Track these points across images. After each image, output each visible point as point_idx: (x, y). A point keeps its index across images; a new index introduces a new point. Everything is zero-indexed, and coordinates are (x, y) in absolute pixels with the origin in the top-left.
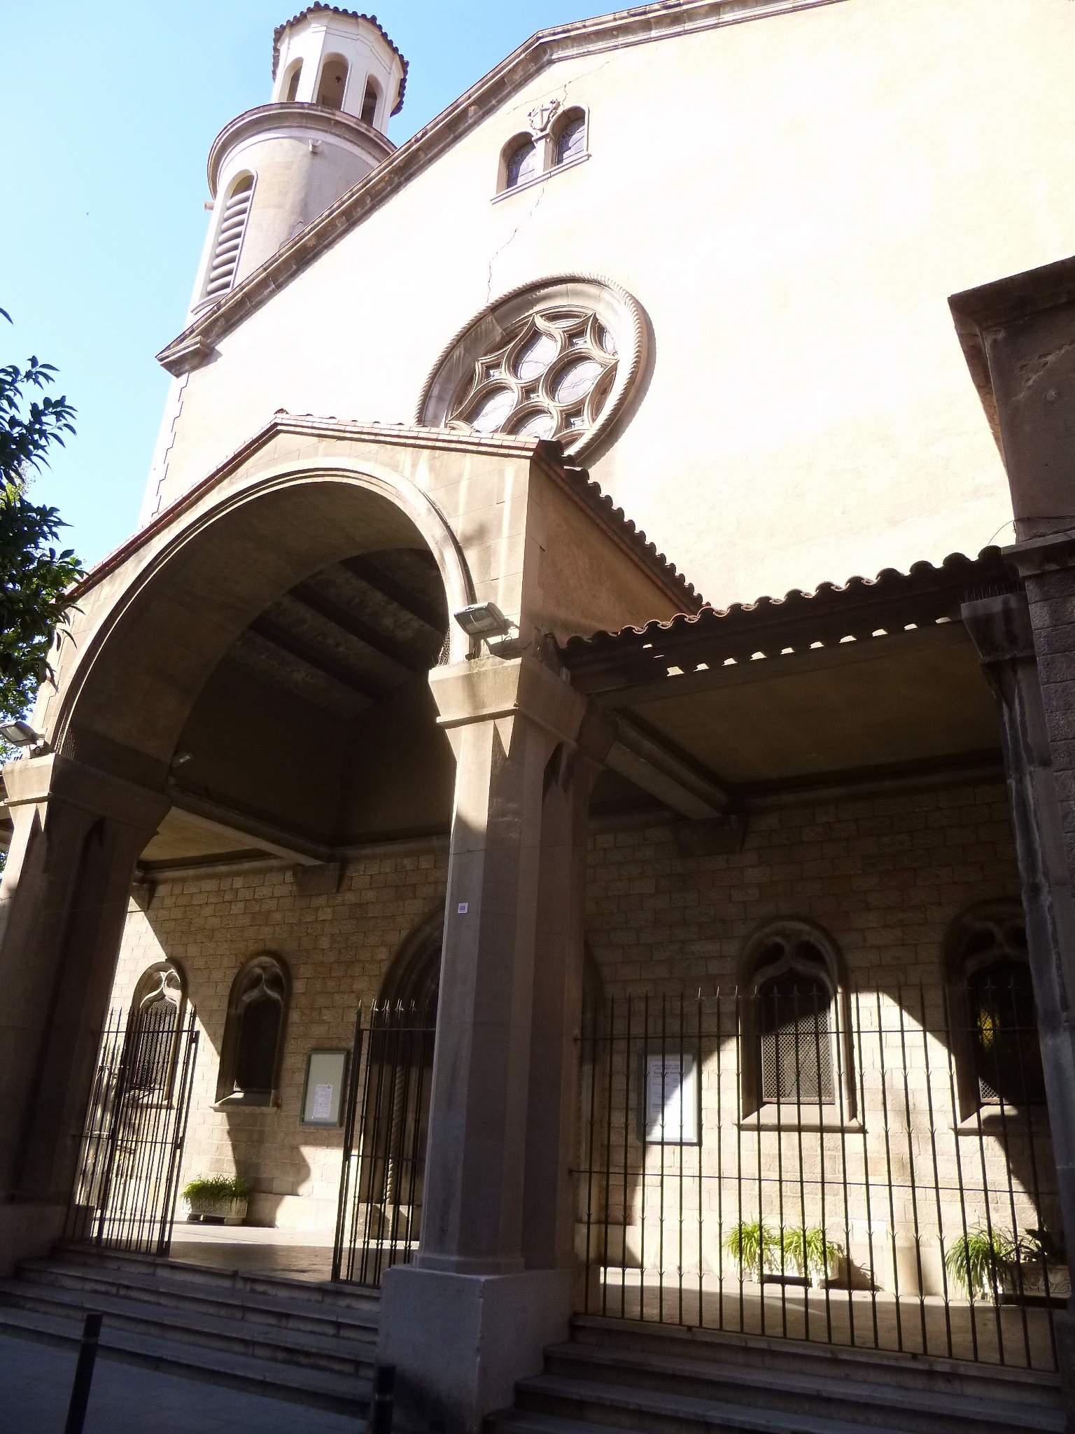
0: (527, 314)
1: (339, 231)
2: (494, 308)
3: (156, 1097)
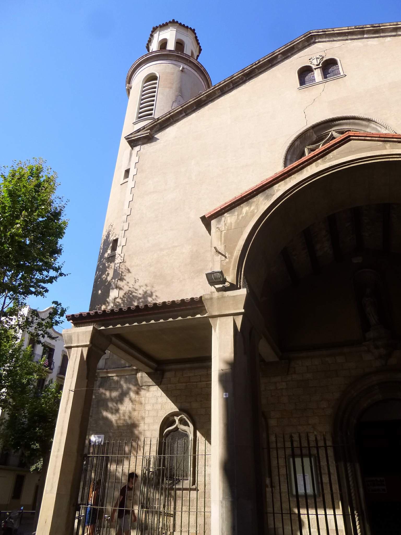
0: (328, 131)
1: (217, 95)
2: (314, 127)
3: (186, 484)
